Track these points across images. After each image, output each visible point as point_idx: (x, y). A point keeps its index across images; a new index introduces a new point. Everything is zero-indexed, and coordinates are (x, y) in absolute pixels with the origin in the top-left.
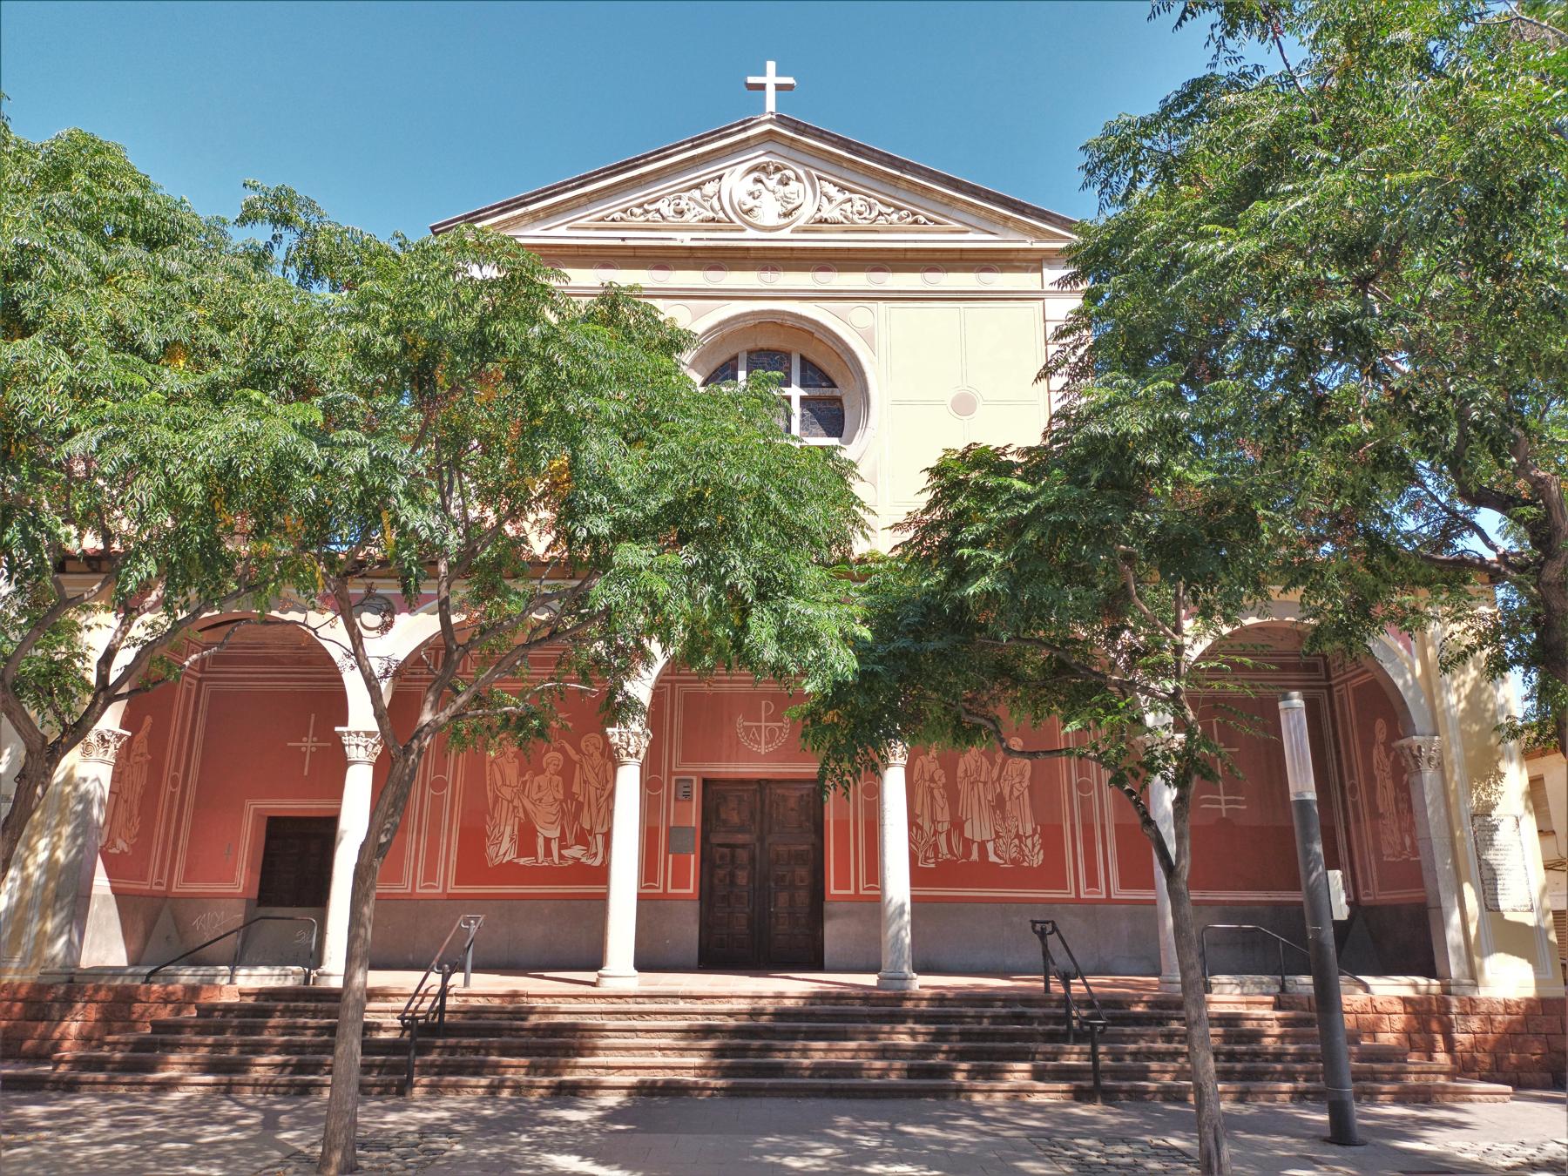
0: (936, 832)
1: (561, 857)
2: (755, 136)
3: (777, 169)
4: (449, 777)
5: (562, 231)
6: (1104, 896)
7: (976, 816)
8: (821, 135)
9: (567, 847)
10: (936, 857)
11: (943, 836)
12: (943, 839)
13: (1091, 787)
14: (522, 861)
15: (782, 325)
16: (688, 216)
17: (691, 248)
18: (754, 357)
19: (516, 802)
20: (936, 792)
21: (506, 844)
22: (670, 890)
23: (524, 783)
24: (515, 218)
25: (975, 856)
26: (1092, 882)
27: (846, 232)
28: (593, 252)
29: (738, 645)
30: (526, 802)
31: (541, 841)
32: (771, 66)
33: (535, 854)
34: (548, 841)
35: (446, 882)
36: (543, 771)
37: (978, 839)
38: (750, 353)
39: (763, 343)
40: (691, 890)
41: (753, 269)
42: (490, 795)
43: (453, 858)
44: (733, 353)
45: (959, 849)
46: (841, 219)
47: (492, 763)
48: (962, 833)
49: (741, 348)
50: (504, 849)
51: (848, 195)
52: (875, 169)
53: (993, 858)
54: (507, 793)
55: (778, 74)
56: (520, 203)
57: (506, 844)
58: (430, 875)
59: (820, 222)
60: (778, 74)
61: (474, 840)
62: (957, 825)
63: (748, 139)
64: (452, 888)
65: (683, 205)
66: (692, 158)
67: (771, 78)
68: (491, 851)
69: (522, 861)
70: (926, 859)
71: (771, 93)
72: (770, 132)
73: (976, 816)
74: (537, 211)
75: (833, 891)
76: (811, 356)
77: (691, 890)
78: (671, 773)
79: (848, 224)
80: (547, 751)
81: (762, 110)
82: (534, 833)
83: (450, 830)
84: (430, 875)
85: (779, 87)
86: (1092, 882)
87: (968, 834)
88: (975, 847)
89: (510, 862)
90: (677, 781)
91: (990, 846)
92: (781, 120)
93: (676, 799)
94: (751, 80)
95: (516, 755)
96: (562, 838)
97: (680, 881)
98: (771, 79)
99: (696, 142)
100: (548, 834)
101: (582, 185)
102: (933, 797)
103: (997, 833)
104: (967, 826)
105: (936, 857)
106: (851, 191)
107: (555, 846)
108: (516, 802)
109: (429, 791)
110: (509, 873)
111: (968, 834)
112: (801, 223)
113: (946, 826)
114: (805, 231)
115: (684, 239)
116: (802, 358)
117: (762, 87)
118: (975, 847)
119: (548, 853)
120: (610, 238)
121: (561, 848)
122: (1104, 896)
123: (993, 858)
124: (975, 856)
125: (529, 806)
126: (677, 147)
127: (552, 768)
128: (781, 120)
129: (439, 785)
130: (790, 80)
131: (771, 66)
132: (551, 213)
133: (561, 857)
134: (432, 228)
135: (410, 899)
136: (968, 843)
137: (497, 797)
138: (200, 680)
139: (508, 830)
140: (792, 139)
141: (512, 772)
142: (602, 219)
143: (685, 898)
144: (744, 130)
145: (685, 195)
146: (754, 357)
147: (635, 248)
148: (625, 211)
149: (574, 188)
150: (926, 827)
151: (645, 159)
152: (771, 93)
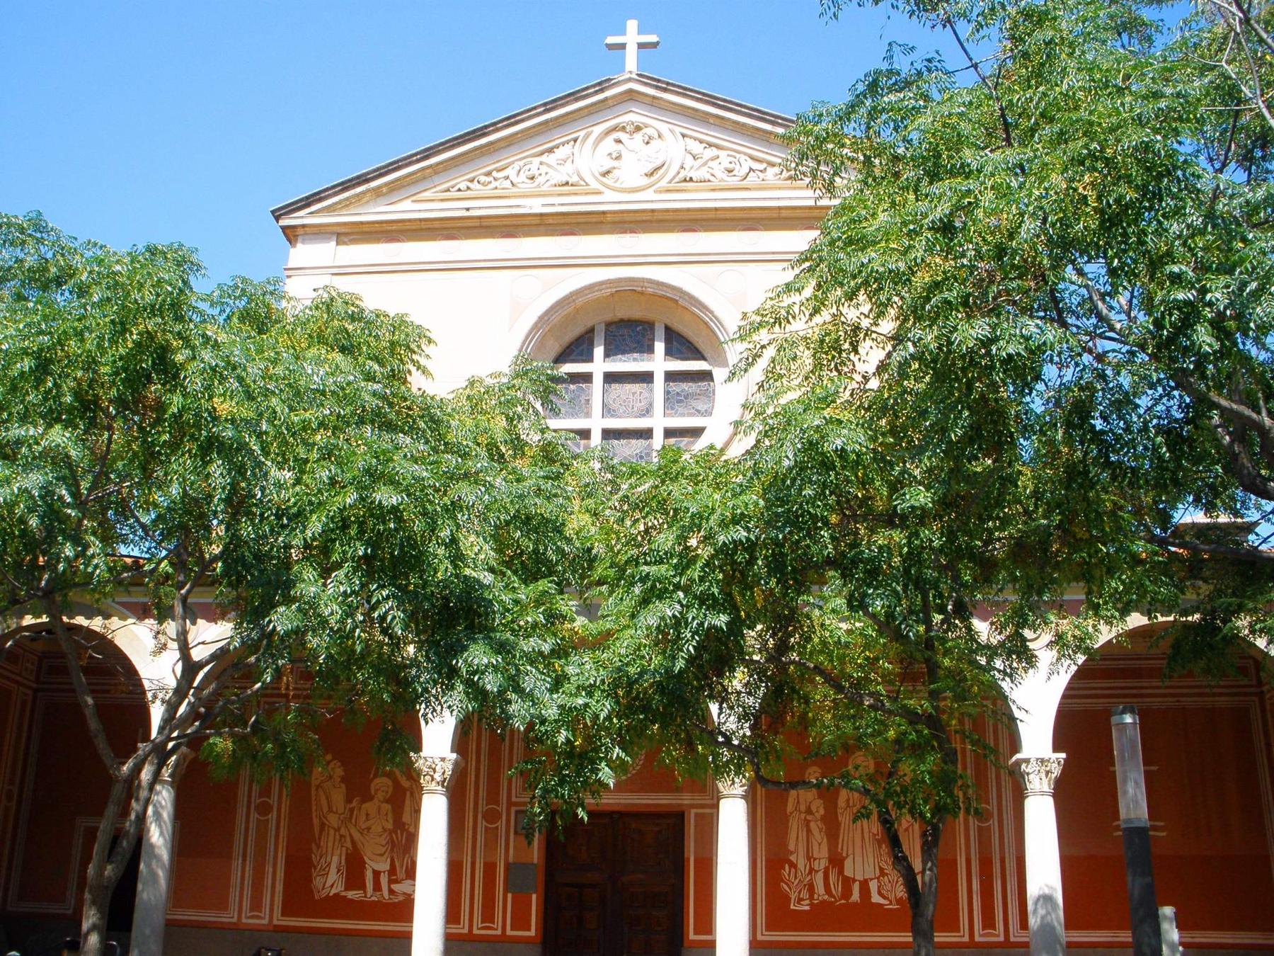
0: (811, 870)
1: (391, 892)
2: (614, 97)
3: (638, 129)
4: (274, 801)
5: (407, 205)
6: (1002, 939)
7: (858, 851)
8: (684, 91)
9: (397, 882)
10: (811, 897)
11: (820, 875)
12: (819, 880)
13: (990, 815)
14: (351, 894)
15: (642, 293)
16: (539, 180)
17: (541, 215)
18: (613, 328)
19: (343, 831)
20: (812, 825)
21: (333, 876)
22: (509, 932)
23: (352, 810)
24: (358, 195)
25: (856, 896)
26: (989, 922)
27: (714, 190)
28: (437, 224)
29: (1076, 540)
30: (353, 830)
31: (369, 875)
32: (632, 25)
33: (363, 887)
34: (377, 874)
35: (271, 914)
36: (371, 798)
37: (859, 877)
38: (609, 325)
39: (623, 313)
40: (532, 933)
41: (612, 232)
42: (316, 821)
43: (279, 887)
44: (589, 325)
45: (837, 890)
46: (708, 176)
47: (318, 787)
48: (841, 872)
49: (598, 319)
50: (331, 881)
51: (714, 152)
52: (744, 125)
53: (876, 898)
54: (333, 820)
55: (640, 33)
56: (363, 179)
57: (333, 876)
58: (256, 905)
59: (685, 180)
60: (640, 33)
61: (300, 870)
62: (836, 861)
63: (606, 99)
64: (279, 920)
65: (534, 171)
66: (546, 122)
67: (632, 36)
68: (318, 882)
69: (351, 894)
70: (800, 900)
71: (631, 55)
72: (631, 91)
73: (858, 851)
74: (379, 187)
75: (692, 936)
76: (677, 326)
77: (532, 933)
78: (510, 804)
79: (715, 183)
80: (376, 776)
81: (622, 70)
82: (362, 864)
83: (275, 857)
84: (256, 905)
85: (641, 46)
86: (989, 922)
87: (848, 872)
88: (856, 889)
89: (336, 895)
90: (517, 812)
91: (873, 886)
92: (642, 78)
93: (516, 833)
94: (611, 40)
95: (343, 780)
96: (392, 871)
97: (520, 920)
98: (632, 36)
99: (549, 106)
100: (377, 867)
101: (427, 157)
102: (809, 831)
103: (881, 870)
104: (848, 865)
105: (811, 897)
106: (718, 147)
107: (384, 880)
108: (343, 831)
109: (254, 816)
110: (336, 906)
111: (848, 872)
112: (663, 183)
113: (824, 863)
114: (668, 191)
115: (536, 206)
116: (667, 329)
117: (587, 378)
118: (856, 889)
119: (377, 887)
120: (454, 209)
121: (391, 882)
122: (1002, 939)
123: (876, 898)
124: (856, 896)
125: (357, 836)
126: (529, 112)
127: (380, 795)
128: (642, 78)
129: (264, 809)
130: (653, 38)
131: (632, 25)
132: (394, 187)
133: (391, 892)
134: (273, 212)
135: (235, 928)
136: (847, 883)
137: (323, 825)
138: (36, 691)
139: (335, 859)
140: (654, 97)
141: (338, 796)
142: (448, 190)
143: (527, 940)
144: (602, 90)
145: (536, 160)
146: (613, 328)
147: (480, 218)
148: (472, 181)
149: (418, 161)
150: (801, 865)
151: (495, 126)
152: (631, 55)
